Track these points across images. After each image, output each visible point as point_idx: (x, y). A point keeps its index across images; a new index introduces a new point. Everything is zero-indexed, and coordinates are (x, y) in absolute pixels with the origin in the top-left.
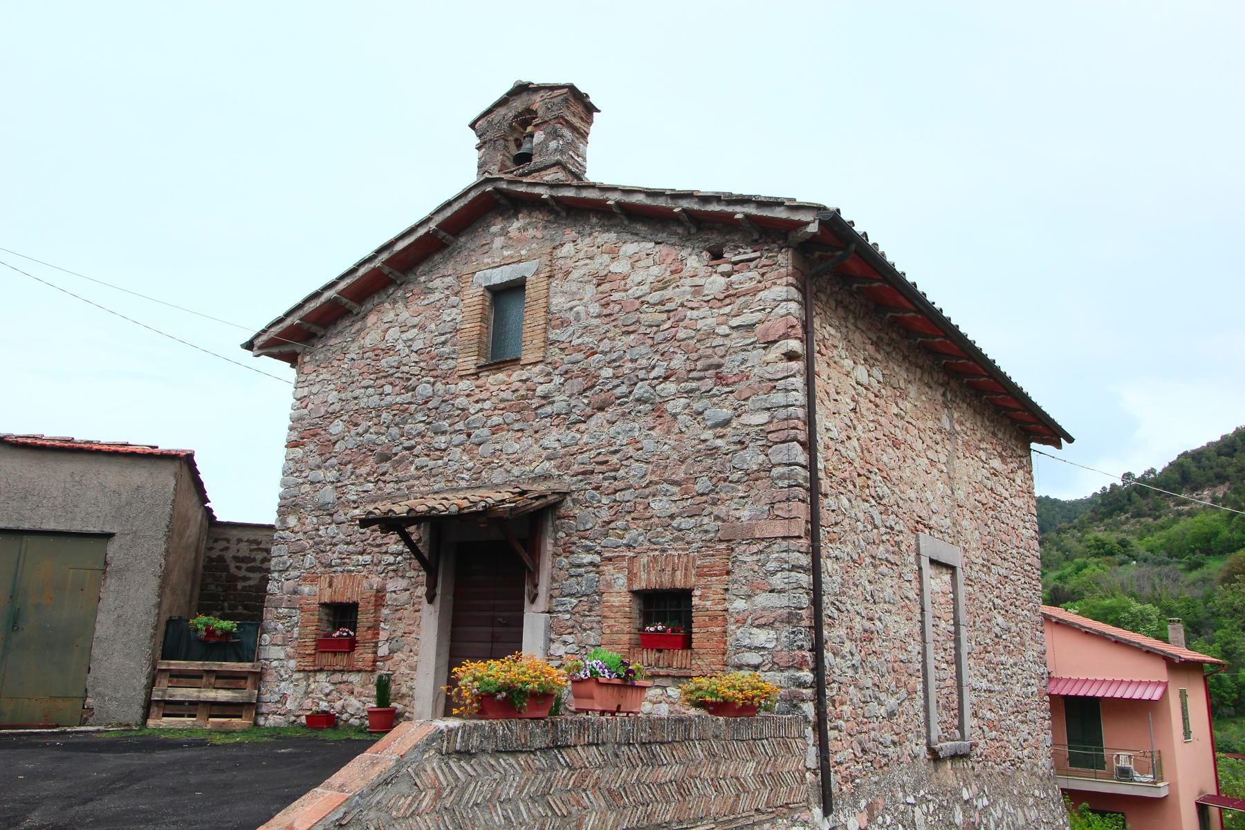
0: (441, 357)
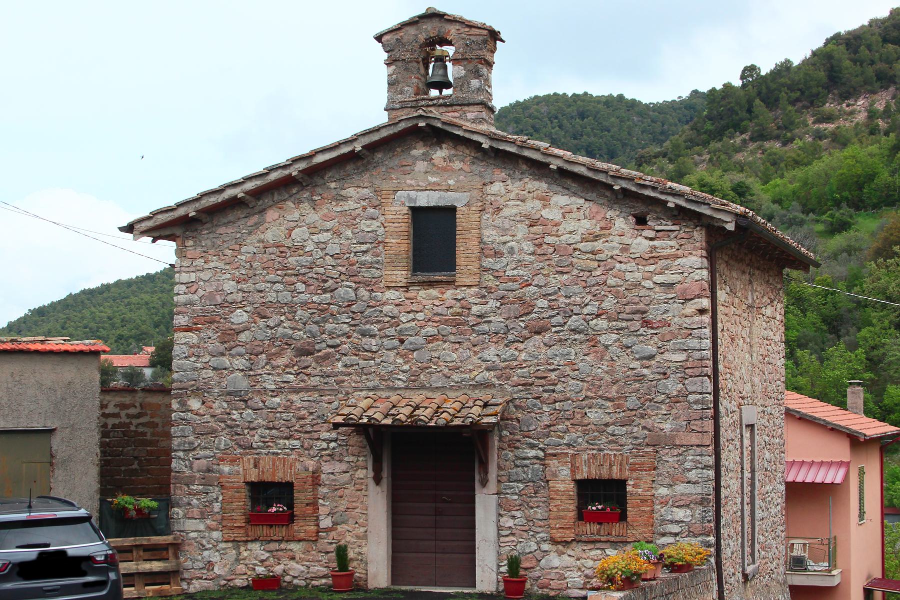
0: (363, 264)
